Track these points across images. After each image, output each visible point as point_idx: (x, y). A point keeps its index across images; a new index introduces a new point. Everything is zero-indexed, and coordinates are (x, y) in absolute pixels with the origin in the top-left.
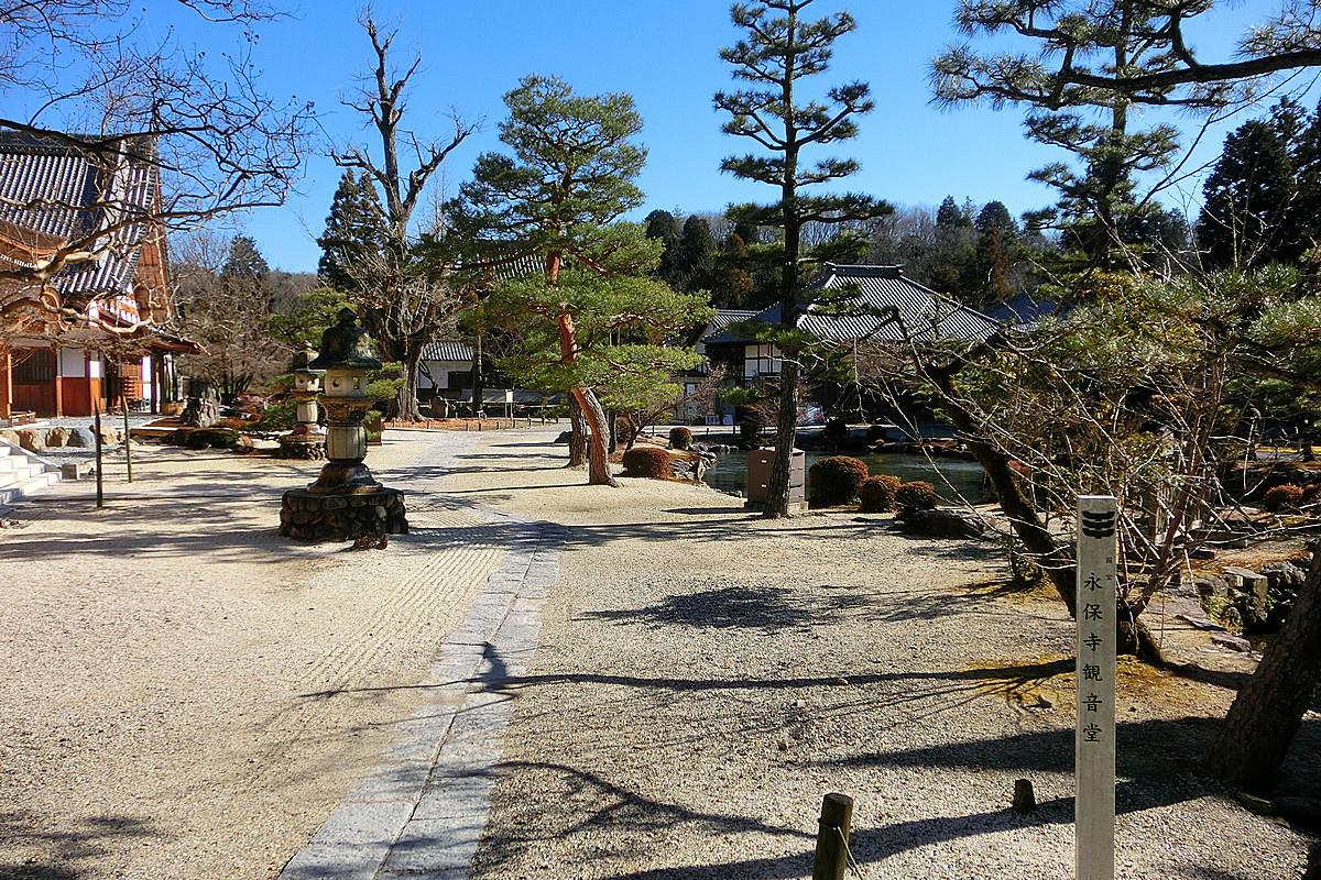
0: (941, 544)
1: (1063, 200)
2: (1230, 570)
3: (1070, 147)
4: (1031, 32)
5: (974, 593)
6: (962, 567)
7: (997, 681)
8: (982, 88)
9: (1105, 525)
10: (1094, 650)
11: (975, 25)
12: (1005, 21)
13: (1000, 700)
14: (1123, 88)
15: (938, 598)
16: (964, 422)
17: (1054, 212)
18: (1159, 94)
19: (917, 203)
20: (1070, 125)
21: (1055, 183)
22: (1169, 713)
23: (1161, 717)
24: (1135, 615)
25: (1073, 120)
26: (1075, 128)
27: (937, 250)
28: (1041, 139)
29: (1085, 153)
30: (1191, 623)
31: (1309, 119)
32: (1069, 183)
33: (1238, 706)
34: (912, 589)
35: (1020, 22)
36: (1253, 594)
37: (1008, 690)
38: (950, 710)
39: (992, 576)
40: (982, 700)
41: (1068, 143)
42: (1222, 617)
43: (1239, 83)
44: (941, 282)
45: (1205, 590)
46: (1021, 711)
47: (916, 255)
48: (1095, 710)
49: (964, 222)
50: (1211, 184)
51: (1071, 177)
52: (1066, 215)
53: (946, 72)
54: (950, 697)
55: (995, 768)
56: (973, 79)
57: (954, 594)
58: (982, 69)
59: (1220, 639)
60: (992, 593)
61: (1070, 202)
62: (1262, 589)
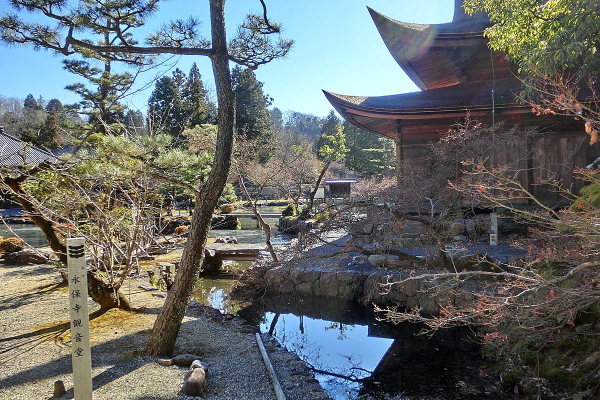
0: (25, 268)
1: (83, 101)
2: (161, 263)
3: (85, 76)
4: (50, 15)
5: (41, 291)
6: (37, 279)
7: (50, 334)
8: (27, 39)
9: (80, 252)
10: (78, 312)
11: (21, 6)
12: (37, 7)
13: (51, 343)
14: (97, 50)
15: (21, 297)
16: (29, 207)
17: (79, 106)
18: (114, 56)
19: (12, 96)
20: (85, 66)
21: (79, 92)
22: (132, 331)
23: (129, 333)
24: (117, 290)
25: (86, 64)
26: (87, 68)
27: (25, 121)
28: (71, 71)
29: (97, 81)
30: (144, 289)
31: (186, 78)
32: (86, 93)
33: (157, 322)
34: (6, 294)
35: (45, 9)
36: (170, 273)
37: (56, 337)
38: (23, 354)
39: (52, 281)
40: (42, 345)
41: (84, 74)
42: (158, 284)
43: (147, 56)
44: (27, 136)
45: (151, 274)
46: (63, 346)
47: (13, 122)
48: (80, 341)
49: (39, 108)
50: (152, 100)
51: (87, 91)
52: (85, 107)
53: (6, 26)
54: (23, 347)
55: (46, 378)
56: (22, 33)
57: (30, 293)
58: (26, 28)
59: (155, 294)
60: (51, 290)
61: (86, 102)
62: (173, 270)
